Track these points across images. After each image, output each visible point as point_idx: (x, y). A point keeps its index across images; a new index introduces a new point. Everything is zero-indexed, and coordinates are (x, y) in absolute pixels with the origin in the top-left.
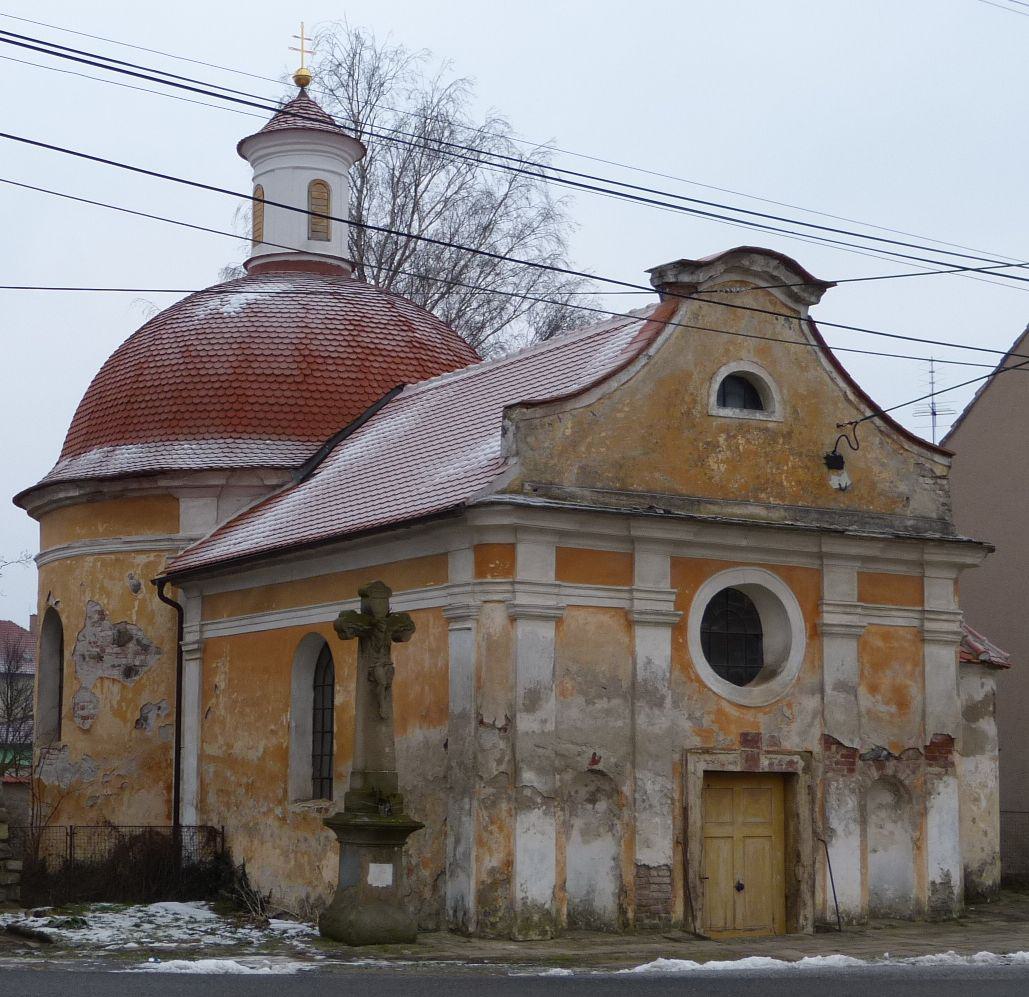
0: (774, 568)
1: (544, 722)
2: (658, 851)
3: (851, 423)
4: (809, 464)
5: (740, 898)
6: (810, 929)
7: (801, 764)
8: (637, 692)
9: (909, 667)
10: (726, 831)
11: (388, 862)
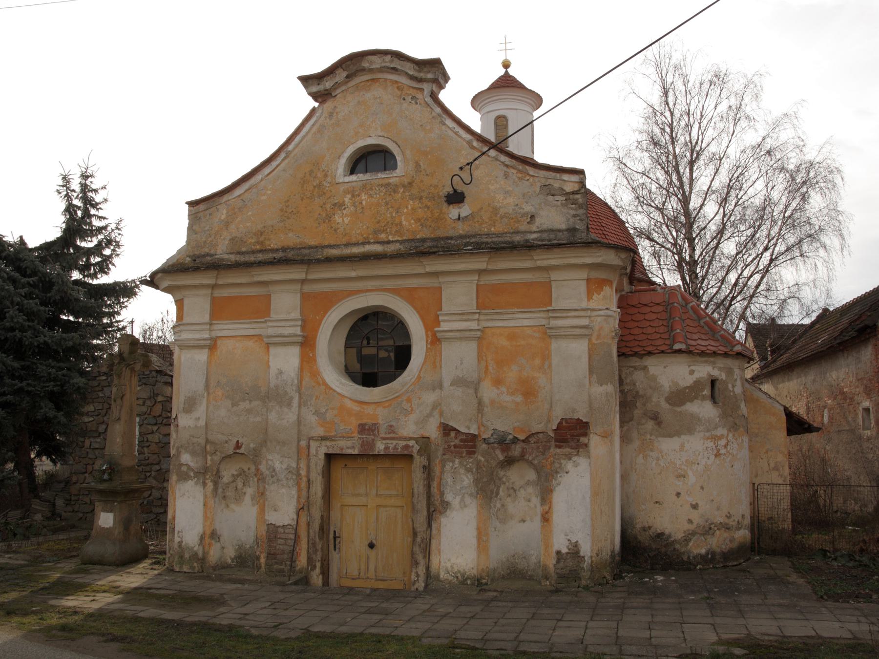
0: (396, 291)
1: (198, 419)
3: (468, 164)
4: (429, 204)
5: (372, 553)
7: (417, 447)
10: (362, 500)
11: (111, 512)
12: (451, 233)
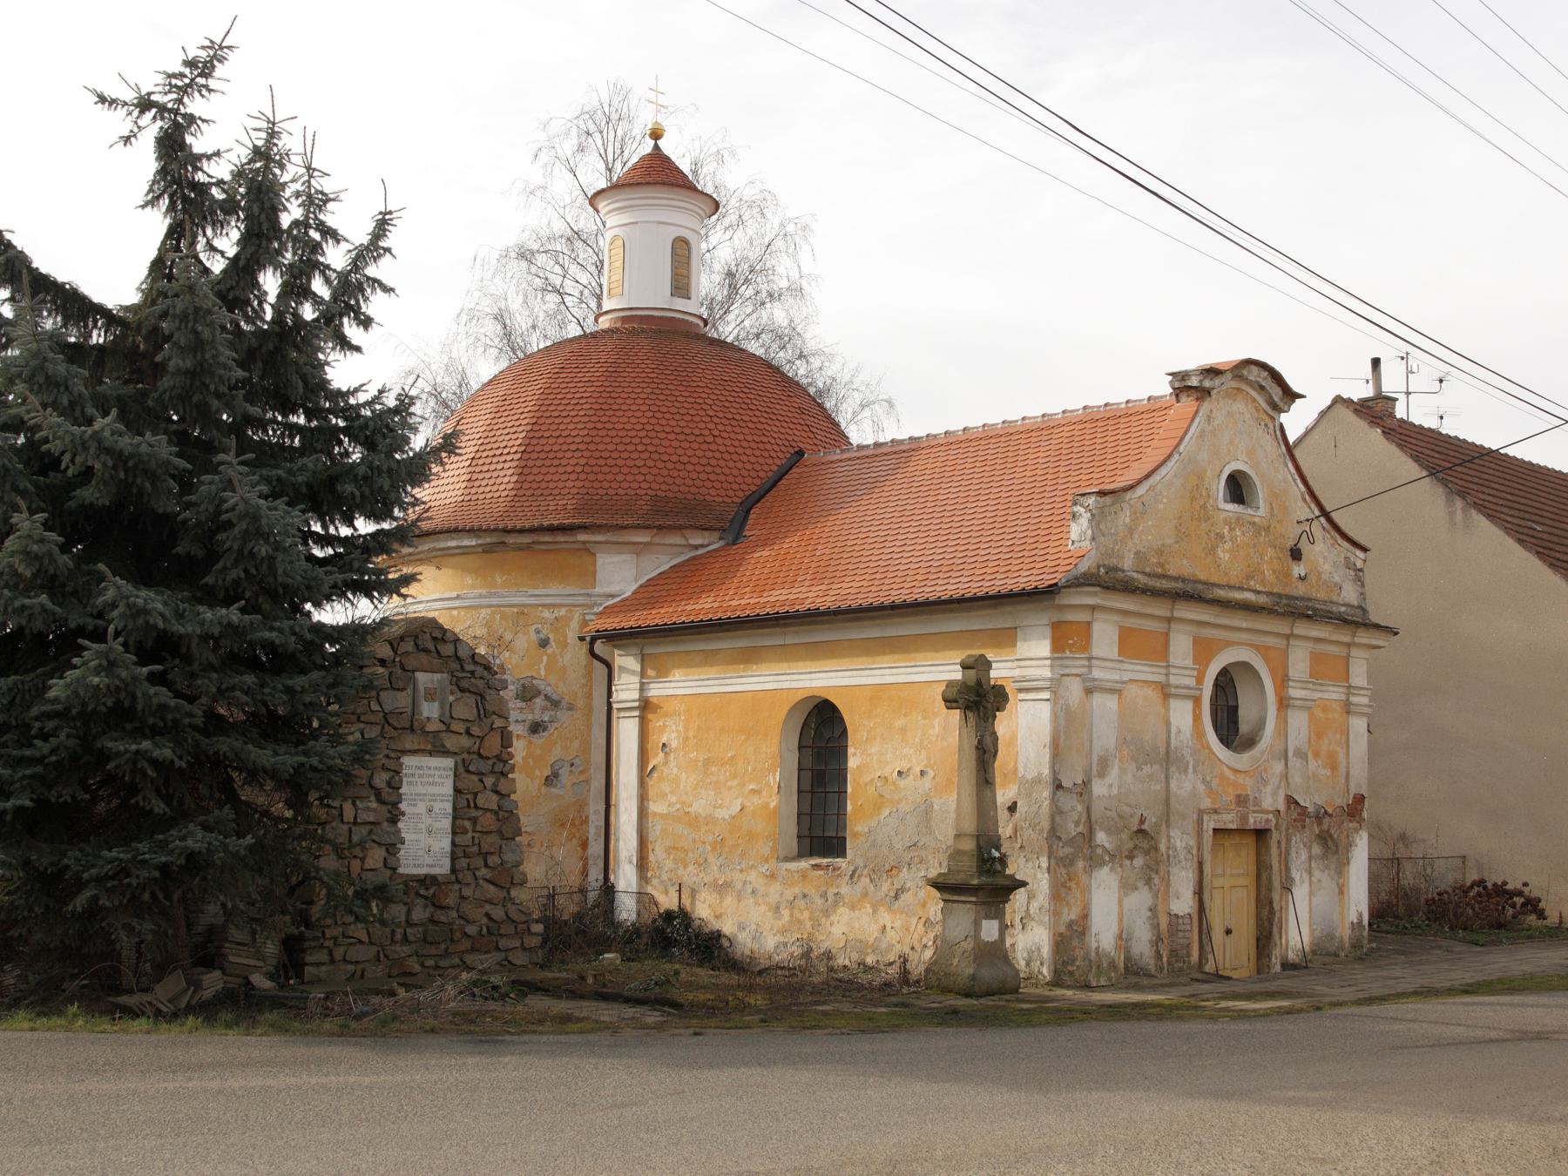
0: (1257, 648)
2: (1183, 904)
3: (1308, 520)
5: (1228, 939)
6: (1278, 968)
8: (1168, 759)
9: (1338, 736)
12: (1294, 593)
